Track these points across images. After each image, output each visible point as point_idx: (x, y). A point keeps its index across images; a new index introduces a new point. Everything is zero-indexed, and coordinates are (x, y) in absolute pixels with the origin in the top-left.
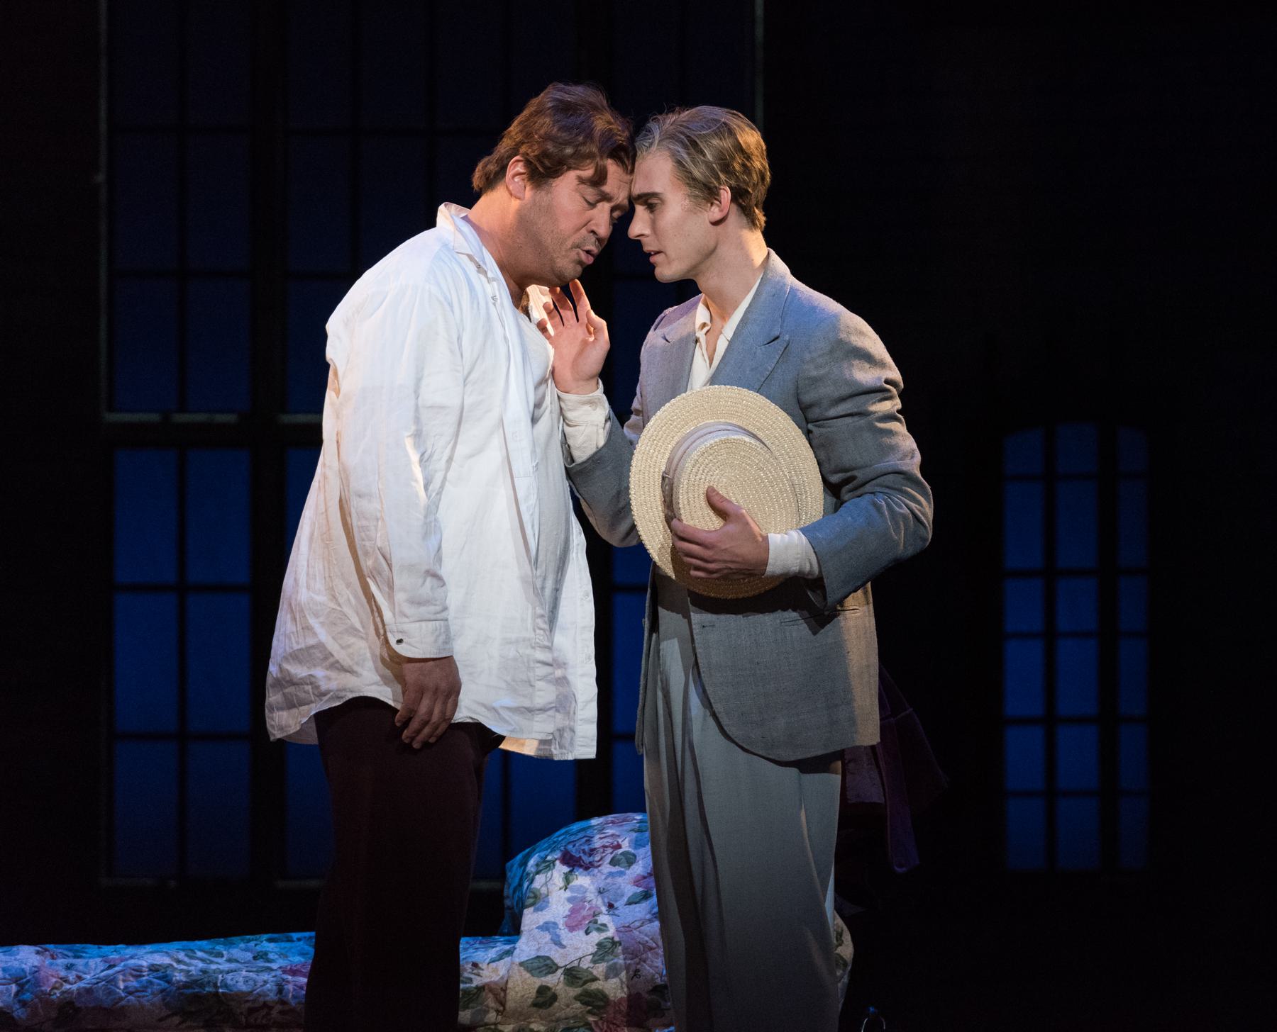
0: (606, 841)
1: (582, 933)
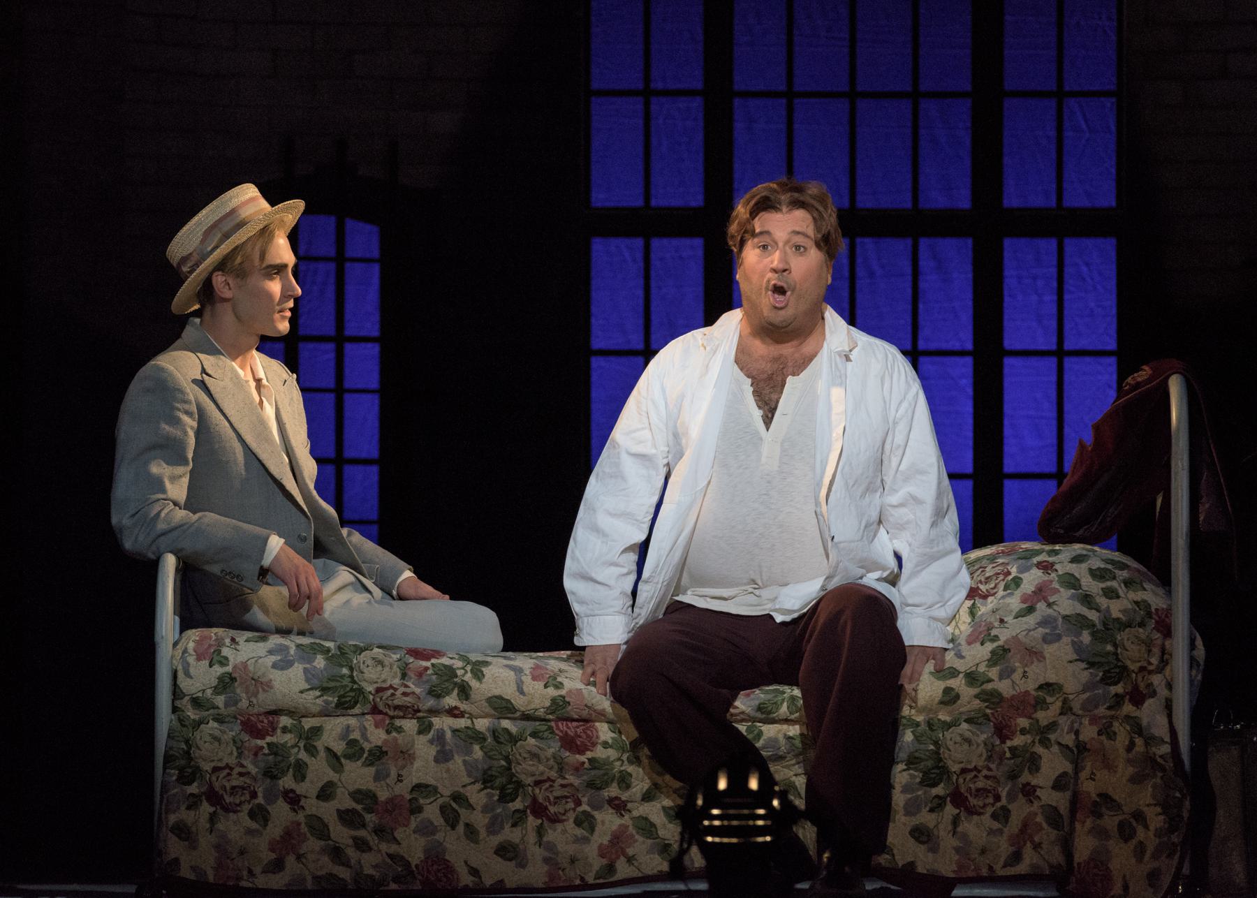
0: (998, 569)
1: (978, 644)
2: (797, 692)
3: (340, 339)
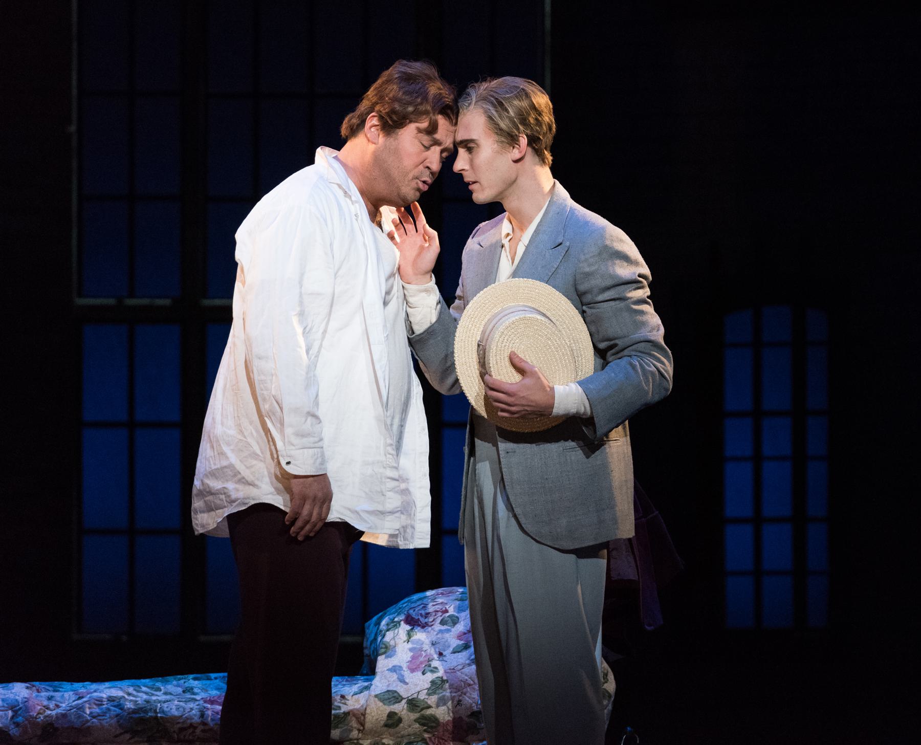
0: (438, 607)
1: (420, 673)
2: (542, 100)
3: (758, 520)
